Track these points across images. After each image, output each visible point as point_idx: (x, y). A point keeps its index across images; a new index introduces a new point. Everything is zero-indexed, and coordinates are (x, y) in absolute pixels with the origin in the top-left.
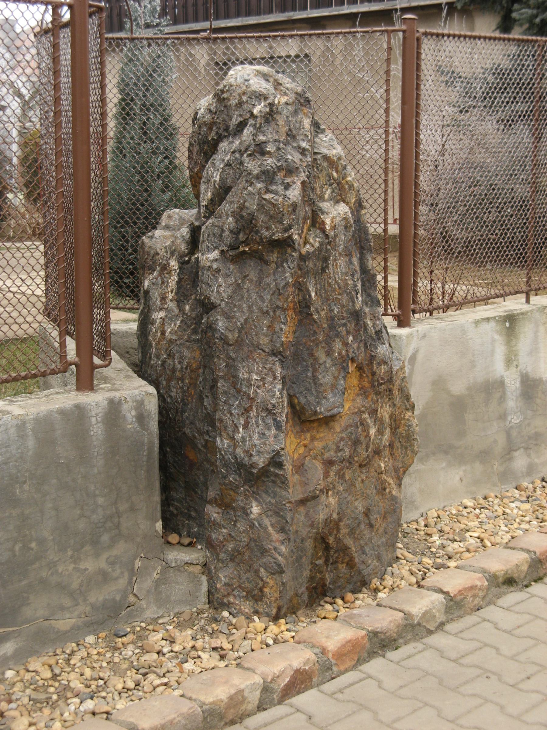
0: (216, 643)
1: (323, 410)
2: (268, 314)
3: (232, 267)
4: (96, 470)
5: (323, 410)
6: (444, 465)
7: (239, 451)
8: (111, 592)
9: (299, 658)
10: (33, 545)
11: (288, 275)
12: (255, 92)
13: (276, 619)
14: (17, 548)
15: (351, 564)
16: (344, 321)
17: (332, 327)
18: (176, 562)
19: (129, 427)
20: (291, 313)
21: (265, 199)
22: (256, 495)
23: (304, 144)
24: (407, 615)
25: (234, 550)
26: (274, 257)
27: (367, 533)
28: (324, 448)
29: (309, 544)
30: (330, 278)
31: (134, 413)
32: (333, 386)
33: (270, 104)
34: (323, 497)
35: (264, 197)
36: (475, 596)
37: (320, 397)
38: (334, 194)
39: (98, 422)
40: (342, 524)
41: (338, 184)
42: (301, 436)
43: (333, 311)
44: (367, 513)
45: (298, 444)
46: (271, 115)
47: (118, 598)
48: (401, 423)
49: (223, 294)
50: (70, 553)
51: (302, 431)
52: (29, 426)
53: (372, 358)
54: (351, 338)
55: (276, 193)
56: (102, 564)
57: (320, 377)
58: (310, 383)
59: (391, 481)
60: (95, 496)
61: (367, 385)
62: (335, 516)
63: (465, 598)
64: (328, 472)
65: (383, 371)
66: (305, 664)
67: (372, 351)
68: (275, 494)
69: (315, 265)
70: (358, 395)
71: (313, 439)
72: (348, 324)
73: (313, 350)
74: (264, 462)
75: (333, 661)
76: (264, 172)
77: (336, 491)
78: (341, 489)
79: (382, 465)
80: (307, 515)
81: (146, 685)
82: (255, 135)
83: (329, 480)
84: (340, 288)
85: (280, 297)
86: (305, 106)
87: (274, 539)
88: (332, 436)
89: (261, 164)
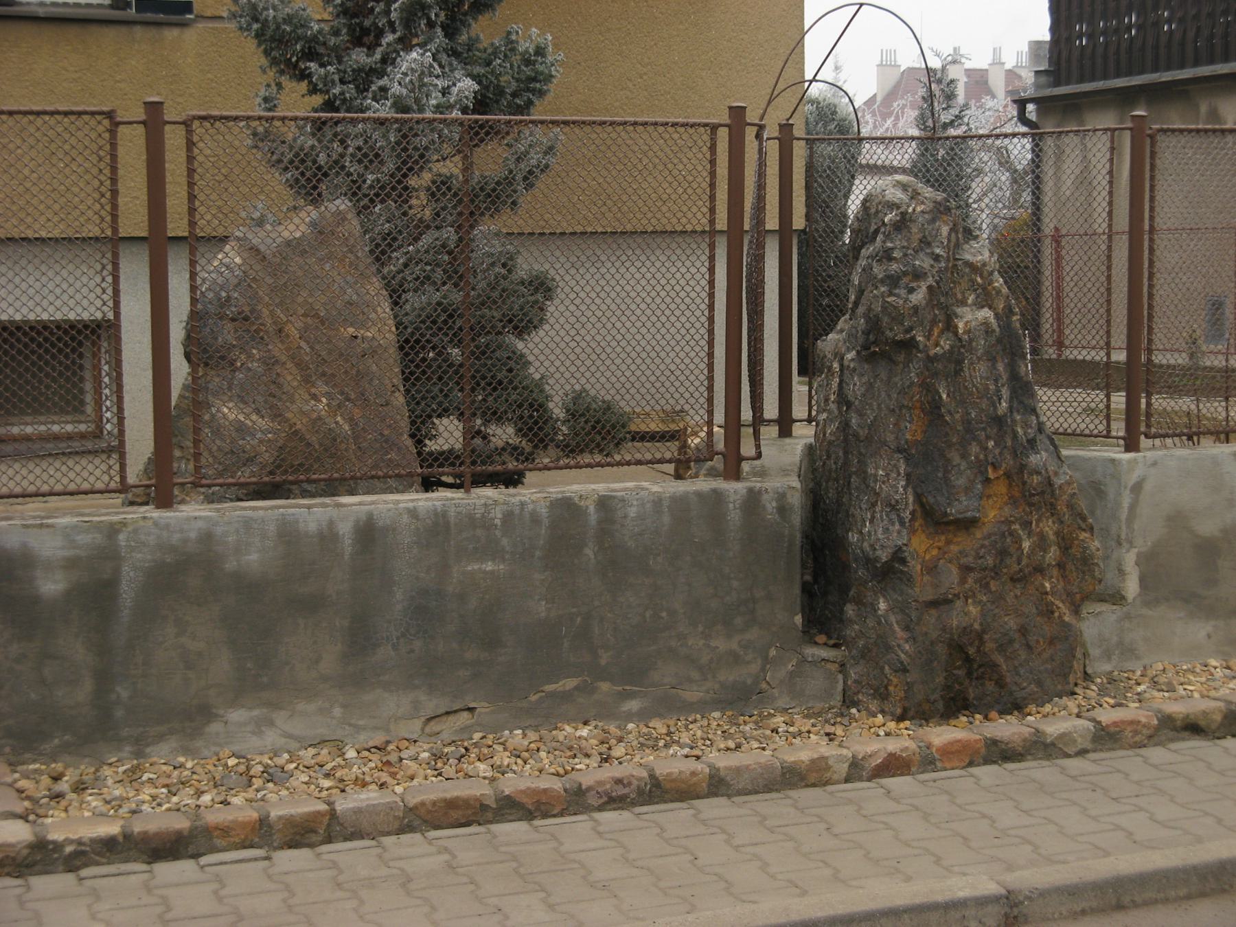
0: (831, 729)
4: (731, 554)
6: (1182, 615)
7: (866, 544)
8: (745, 673)
10: (664, 614)
13: (900, 719)
14: (648, 615)
15: (1000, 683)
17: (968, 430)
20: (917, 412)
23: (938, 251)
26: (901, 358)
27: (1023, 655)
28: (960, 552)
29: (941, 649)
32: (967, 490)
33: (902, 213)
34: (959, 603)
36: (1136, 732)
39: (735, 508)
40: (986, 637)
41: (984, 289)
44: (1023, 631)
46: (903, 224)
47: (749, 681)
50: (700, 628)
51: (937, 533)
52: (666, 503)
53: (1022, 468)
54: (991, 444)
55: (898, 296)
56: (734, 645)
59: (1061, 605)
61: (1017, 494)
62: (977, 626)
66: (901, 751)
70: (1006, 504)
71: (948, 542)
75: (937, 756)
76: (888, 277)
78: (984, 599)
79: (1047, 585)
81: (745, 746)
82: (884, 242)
83: (967, 586)
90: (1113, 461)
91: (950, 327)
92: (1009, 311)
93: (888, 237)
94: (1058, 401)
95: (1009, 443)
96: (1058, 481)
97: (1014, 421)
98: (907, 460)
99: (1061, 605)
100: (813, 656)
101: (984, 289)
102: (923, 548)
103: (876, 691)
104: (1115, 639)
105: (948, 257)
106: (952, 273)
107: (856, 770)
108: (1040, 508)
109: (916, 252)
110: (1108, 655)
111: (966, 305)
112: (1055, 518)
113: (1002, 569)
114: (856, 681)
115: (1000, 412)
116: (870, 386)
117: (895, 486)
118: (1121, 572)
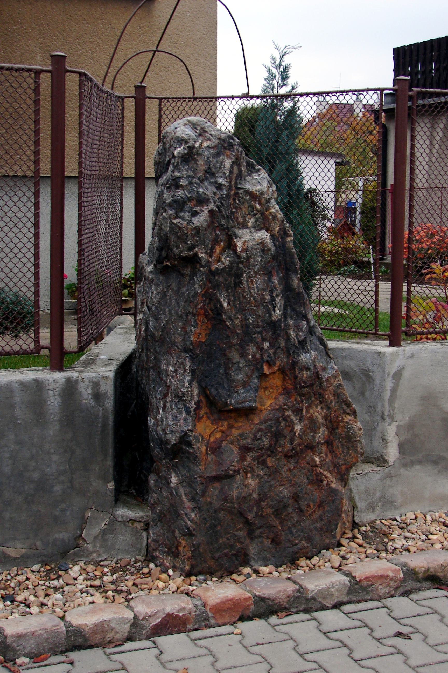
1: (233, 402)
2: (182, 318)
3: (161, 278)
5: (233, 402)
7: (159, 428)
9: (175, 605)
11: (196, 286)
12: (178, 137)
16: (259, 330)
18: (122, 518)
19: (85, 402)
21: (174, 223)
22: (175, 467)
23: (220, 180)
24: (301, 589)
25: (161, 512)
26: (188, 271)
28: (240, 435)
30: (245, 292)
31: (90, 391)
32: (245, 384)
33: (189, 147)
34: (239, 478)
35: (174, 221)
37: (232, 390)
38: (258, 223)
41: (263, 214)
42: (219, 423)
43: (248, 319)
44: (296, 498)
45: (215, 429)
46: (190, 156)
48: (339, 425)
49: (154, 300)
51: (220, 419)
53: (294, 365)
54: (266, 345)
55: (182, 218)
57: (233, 374)
58: (222, 379)
60: (49, 453)
61: (290, 387)
62: (255, 496)
63: (372, 585)
64: (245, 457)
65: (305, 376)
66: (179, 611)
67: (294, 358)
68: (189, 470)
69: (226, 280)
70: (281, 394)
71: (230, 427)
72: (264, 333)
73: (225, 351)
74: (175, 440)
75: (210, 614)
76: (175, 201)
77: (256, 474)
78: (262, 473)
79: (317, 459)
80: (221, 490)
82: (173, 172)
83: (246, 463)
84: (256, 301)
85: (191, 304)
86: (229, 150)
87: (186, 506)
88: (250, 426)
89: (174, 195)
90: (379, 353)
91: (230, 245)
92: (284, 233)
93: (176, 167)
94: (358, 295)
95: (283, 344)
96: (325, 375)
97: (287, 325)
98: (192, 359)
99: (329, 475)
100: (123, 516)
101: (263, 214)
102: (209, 431)
103: (169, 549)
104: (378, 494)
105: (230, 186)
106: (234, 200)
107: (137, 630)
108: (310, 397)
109: (202, 181)
110: (372, 507)
111: (247, 227)
112: (323, 405)
113: (276, 445)
114: (154, 540)
115: (274, 318)
116: (164, 295)
117: (182, 381)
118: (384, 441)
